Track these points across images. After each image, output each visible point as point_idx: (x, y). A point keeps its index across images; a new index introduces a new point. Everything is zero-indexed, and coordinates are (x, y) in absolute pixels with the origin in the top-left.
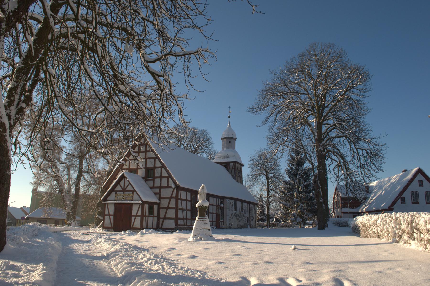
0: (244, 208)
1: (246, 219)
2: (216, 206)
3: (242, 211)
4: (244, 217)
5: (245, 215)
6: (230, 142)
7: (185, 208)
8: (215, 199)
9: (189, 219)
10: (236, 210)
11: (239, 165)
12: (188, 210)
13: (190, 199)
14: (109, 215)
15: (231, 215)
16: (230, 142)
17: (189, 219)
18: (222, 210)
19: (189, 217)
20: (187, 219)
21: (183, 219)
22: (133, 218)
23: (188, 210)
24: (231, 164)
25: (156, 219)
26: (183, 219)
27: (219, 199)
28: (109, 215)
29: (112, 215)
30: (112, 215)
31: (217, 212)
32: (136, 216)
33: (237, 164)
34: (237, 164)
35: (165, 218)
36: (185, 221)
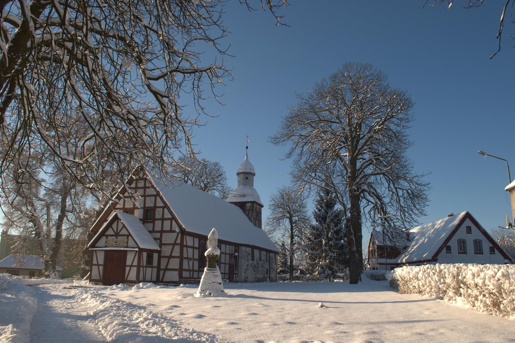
0: (263, 258)
1: (265, 271)
2: (229, 254)
3: (260, 260)
4: (262, 269)
5: (264, 266)
6: (247, 178)
7: (192, 257)
8: (228, 247)
9: (196, 271)
10: (253, 259)
11: (258, 206)
12: (196, 260)
13: (197, 246)
14: (98, 265)
15: (247, 266)
16: (247, 178)
17: (196, 271)
18: (236, 259)
19: (196, 268)
20: (193, 271)
21: (189, 270)
22: (127, 269)
23: (196, 260)
24: (248, 205)
25: (155, 270)
26: (189, 270)
27: (233, 247)
28: (98, 265)
29: (101, 265)
30: (101, 265)
31: (230, 262)
32: (131, 266)
33: (255, 205)
34: (255, 205)
35: (166, 269)
36: (191, 273)
